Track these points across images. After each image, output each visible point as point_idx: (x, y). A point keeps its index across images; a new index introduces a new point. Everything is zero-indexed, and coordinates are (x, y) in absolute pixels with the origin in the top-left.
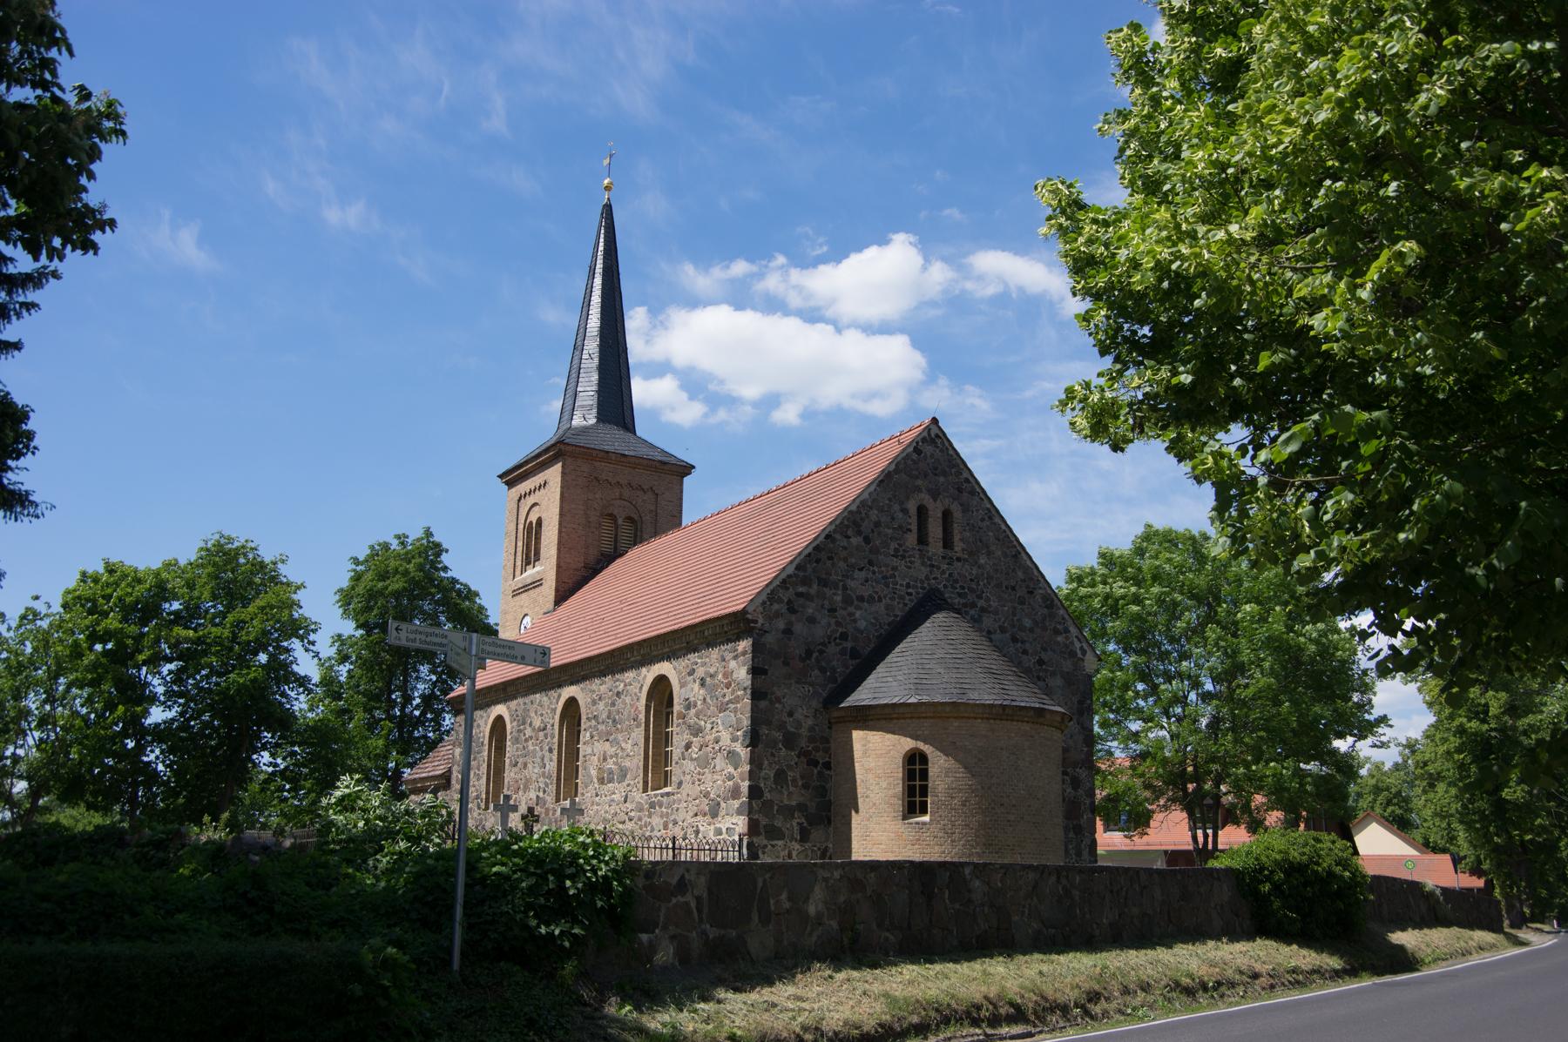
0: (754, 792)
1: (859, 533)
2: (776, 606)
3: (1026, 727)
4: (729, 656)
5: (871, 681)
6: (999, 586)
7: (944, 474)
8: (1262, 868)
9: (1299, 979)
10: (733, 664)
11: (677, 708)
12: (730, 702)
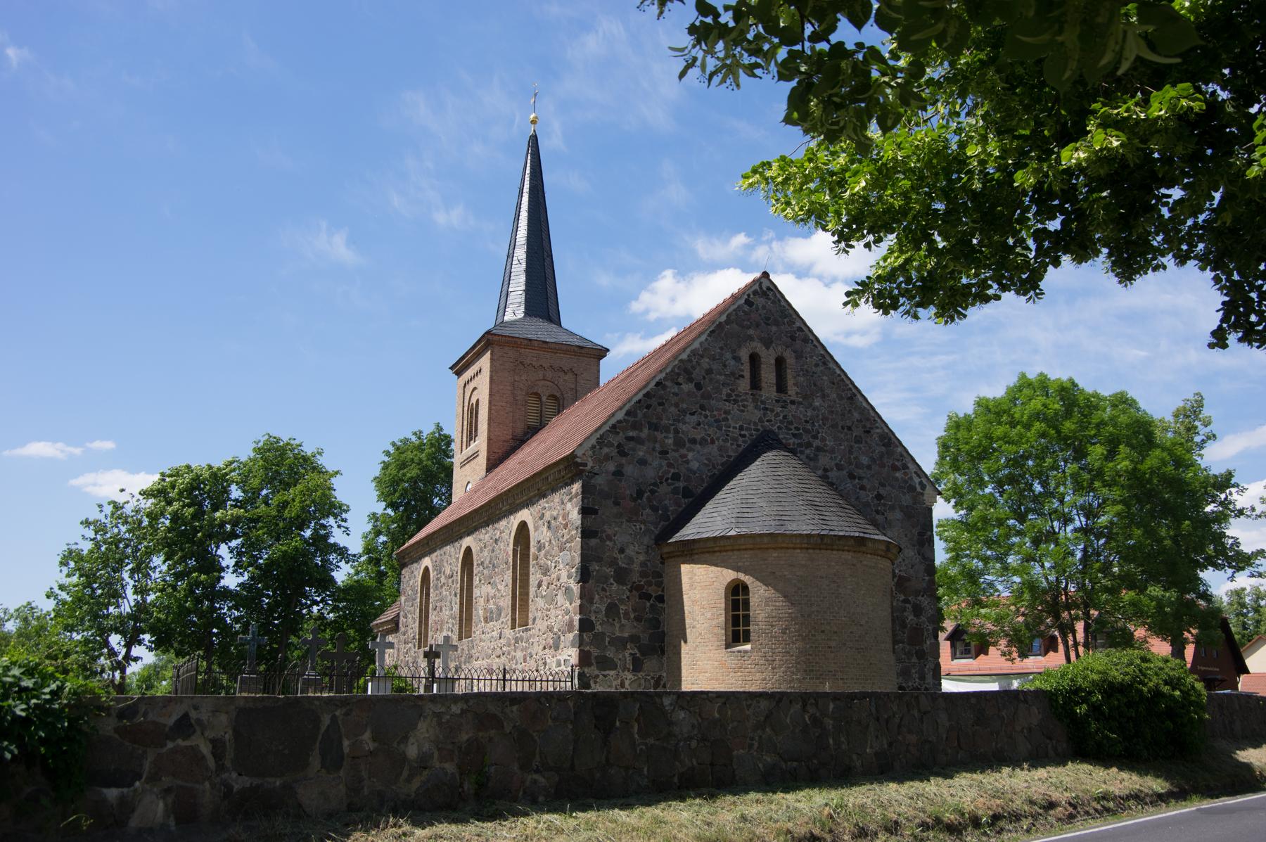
0: (585, 625)
1: (690, 380)
2: (606, 450)
3: (848, 556)
4: (566, 498)
5: (699, 518)
6: (834, 426)
7: (777, 323)
8: (1080, 689)
9: (1108, 806)
10: (569, 505)
11: (533, 550)
12: (567, 541)
